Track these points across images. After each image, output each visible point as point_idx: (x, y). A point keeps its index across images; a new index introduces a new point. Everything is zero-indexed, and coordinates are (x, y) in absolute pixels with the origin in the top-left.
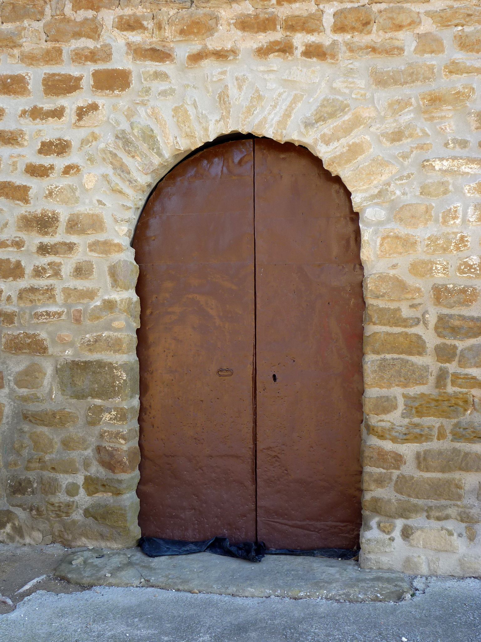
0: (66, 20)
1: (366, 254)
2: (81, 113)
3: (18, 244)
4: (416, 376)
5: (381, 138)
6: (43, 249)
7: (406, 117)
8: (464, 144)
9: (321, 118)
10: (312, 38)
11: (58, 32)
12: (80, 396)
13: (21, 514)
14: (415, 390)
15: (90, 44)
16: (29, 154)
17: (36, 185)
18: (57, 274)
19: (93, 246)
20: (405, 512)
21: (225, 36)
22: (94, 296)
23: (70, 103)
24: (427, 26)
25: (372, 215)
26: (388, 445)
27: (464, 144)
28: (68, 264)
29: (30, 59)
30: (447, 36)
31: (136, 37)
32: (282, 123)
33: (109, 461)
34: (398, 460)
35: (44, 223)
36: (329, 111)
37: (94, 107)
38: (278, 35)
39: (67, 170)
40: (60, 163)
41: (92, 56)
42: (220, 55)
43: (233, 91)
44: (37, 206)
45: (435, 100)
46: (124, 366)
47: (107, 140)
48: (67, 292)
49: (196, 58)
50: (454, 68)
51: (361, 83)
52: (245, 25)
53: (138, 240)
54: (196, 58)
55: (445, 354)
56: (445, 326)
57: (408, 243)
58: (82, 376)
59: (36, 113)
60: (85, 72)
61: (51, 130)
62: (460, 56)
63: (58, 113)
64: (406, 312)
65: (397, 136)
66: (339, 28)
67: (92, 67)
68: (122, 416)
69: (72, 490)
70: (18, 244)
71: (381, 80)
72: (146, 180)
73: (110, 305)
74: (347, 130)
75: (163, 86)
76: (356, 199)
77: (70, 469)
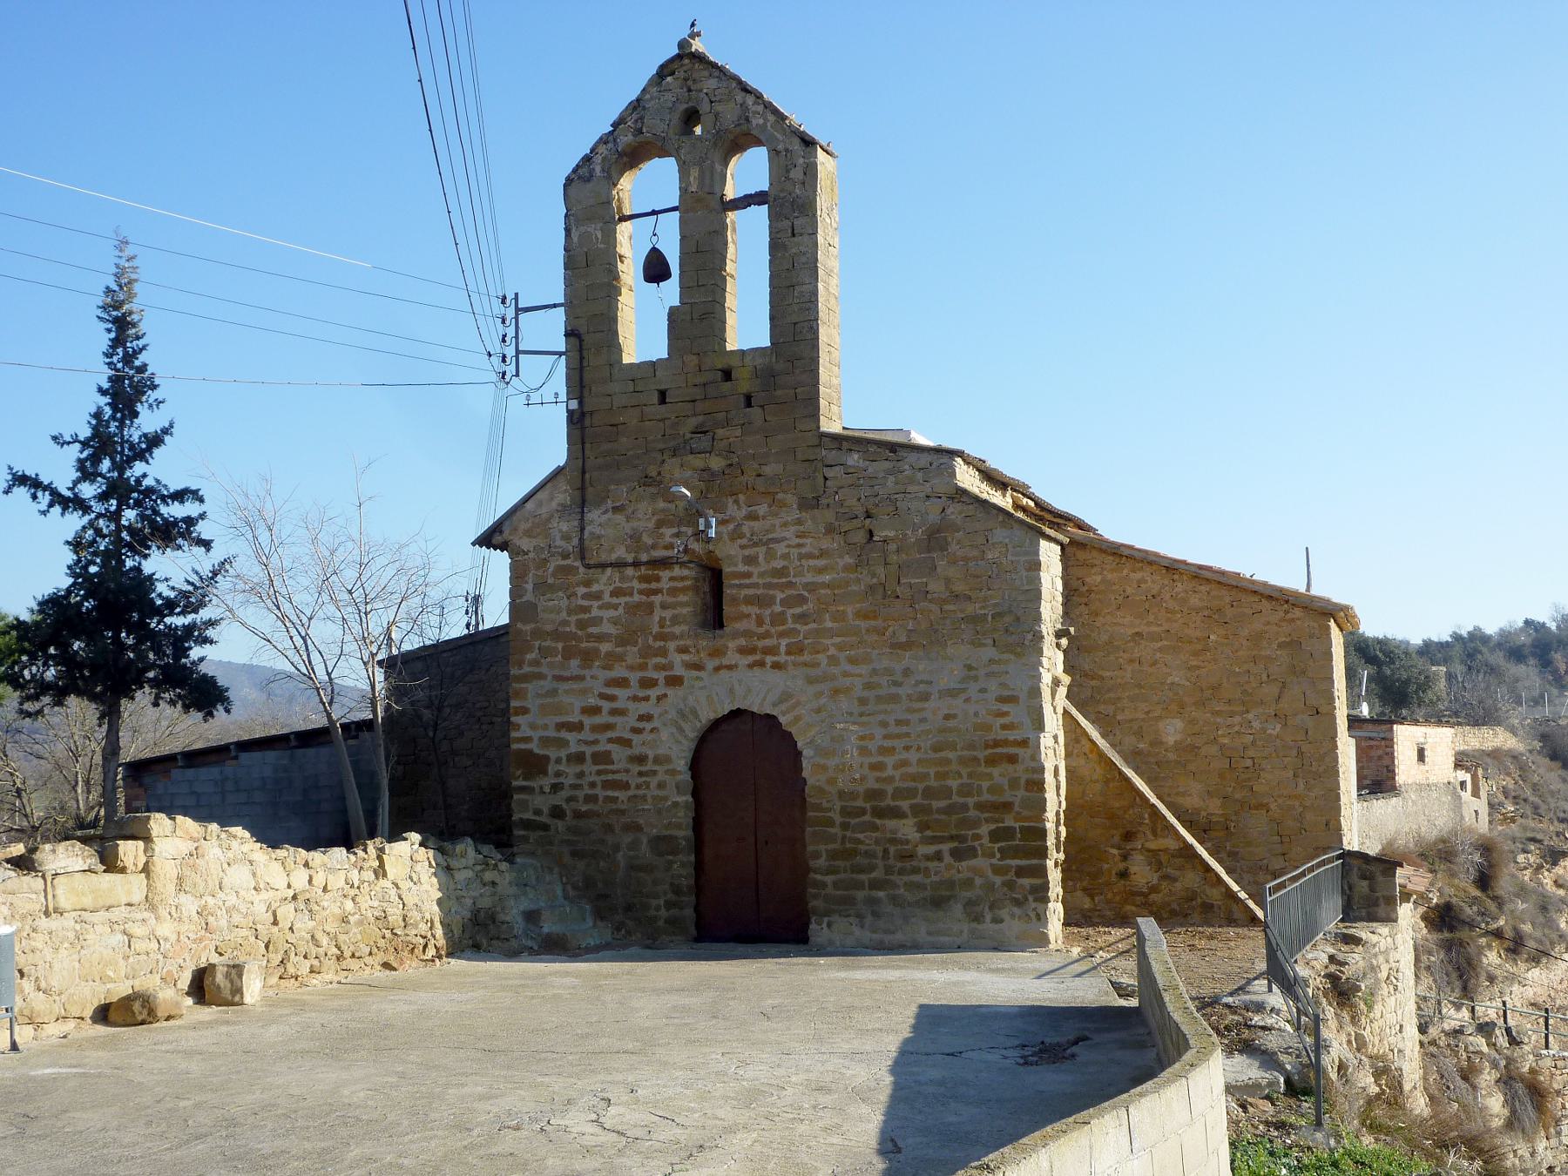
0: (649, 647)
1: (805, 774)
2: (659, 699)
3: (627, 771)
4: (831, 839)
5: (1290, 616)
6: (641, 774)
7: (823, 701)
8: (851, 714)
9: (781, 702)
10: (775, 659)
11: (647, 652)
12: (660, 854)
13: (630, 923)
14: (831, 846)
15: (663, 661)
16: (632, 721)
17: (636, 739)
18: (648, 787)
19: (667, 772)
20: (827, 913)
21: (732, 657)
22: (667, 797)
23: (653, 693)
24: (832, 651)
25: (807, 752)
26: (819, 877)
27: (851, 714)
28: (654, 781)
29: (631, 668)
30: (842, 656)
31: (686, 657)
32: (761, 704)
33: (677, 890)
34: (824, 885)
35: (641, 759)
36: (785, 697)
37: (665, 695)
38: (757, 657)
39: (652, 731)
40: (648, 726)
41: (663, 668)
42: (730, 667)
43: (737, 687)
44: (637, 751)
45: (836, 692)
46: (684, 838)
47: (673, 714)
48: (654, 798)
49: (717, 669)
50: (846, 674)
51: (800, 682)
52: (743, 651)
53: (695, 765)
54: (717, 669)
55: (845, 826)
56: (845, 812)
57: (824, 768)
58: (663, 844)
59: (635, 699)
60: (660, 676)
61: (643, 708)
62: (848, 667)
63: (647, 699)
64: (825, 805)
65: (818, 711)
66: (788, 653)
67: (665, 673)
68: (683, 865)
69: (658, 908)
70: (627, 771)
71: (811, 681)
72: (693, 735)
73: (676, 804)
74: (794, 707)
75: (701, 684)
76: (799, 745)
77: (657, 897)
